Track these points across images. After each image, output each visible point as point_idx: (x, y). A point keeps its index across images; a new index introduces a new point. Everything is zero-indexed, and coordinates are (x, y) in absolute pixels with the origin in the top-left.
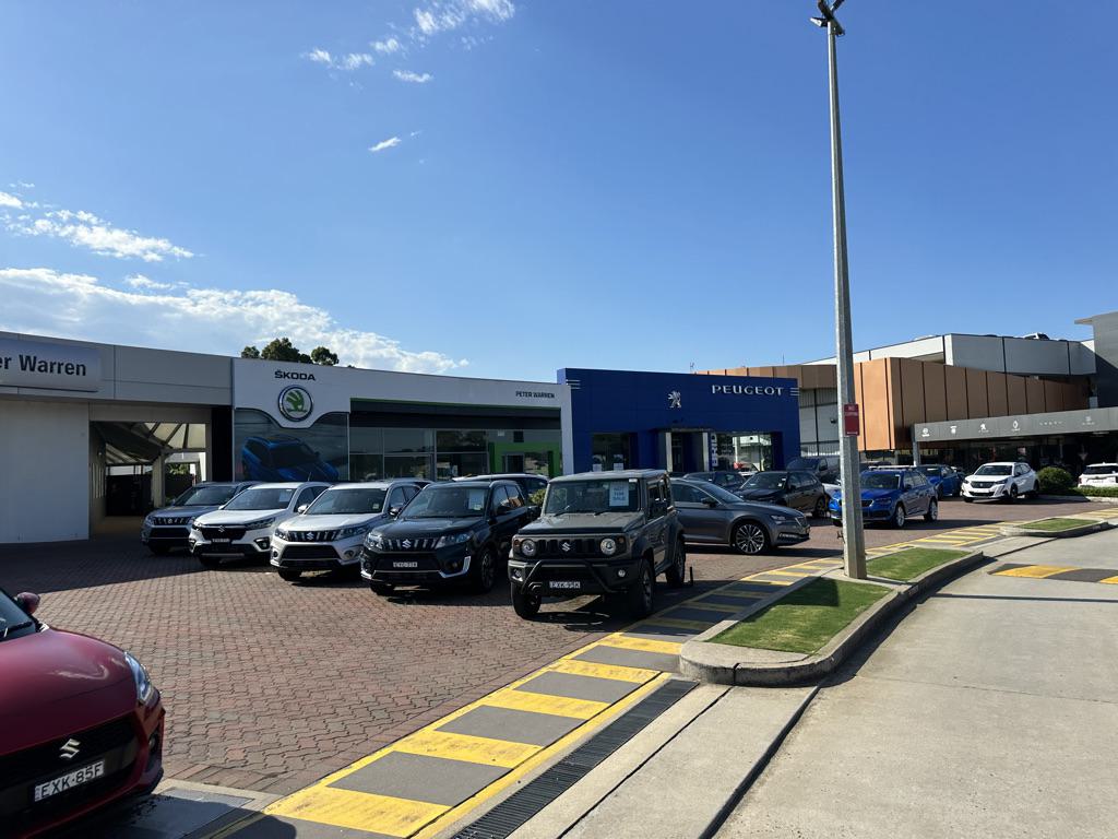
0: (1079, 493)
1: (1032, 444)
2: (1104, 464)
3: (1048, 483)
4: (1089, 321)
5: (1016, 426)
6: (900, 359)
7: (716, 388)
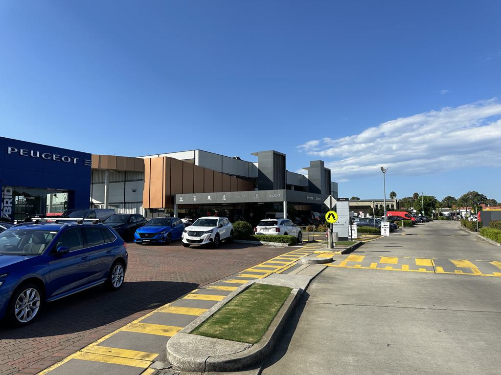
0: (256, 239)
1: (231, 208)
2: (269, 220)
3: (239, 231)
4: (257, 154)
5: (225, 198)
6: (171, 158)
7: (12, 150)
